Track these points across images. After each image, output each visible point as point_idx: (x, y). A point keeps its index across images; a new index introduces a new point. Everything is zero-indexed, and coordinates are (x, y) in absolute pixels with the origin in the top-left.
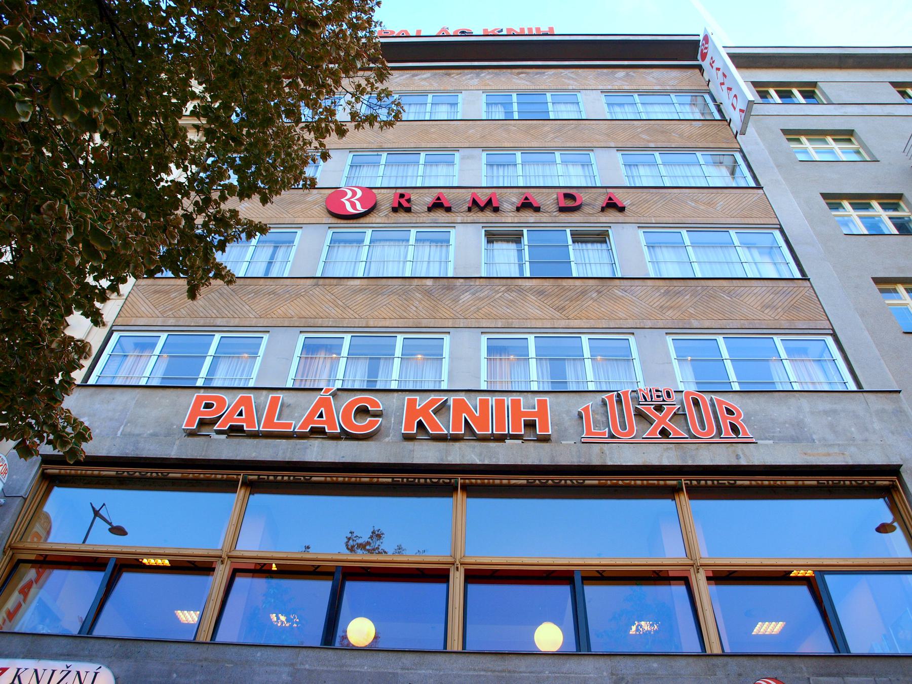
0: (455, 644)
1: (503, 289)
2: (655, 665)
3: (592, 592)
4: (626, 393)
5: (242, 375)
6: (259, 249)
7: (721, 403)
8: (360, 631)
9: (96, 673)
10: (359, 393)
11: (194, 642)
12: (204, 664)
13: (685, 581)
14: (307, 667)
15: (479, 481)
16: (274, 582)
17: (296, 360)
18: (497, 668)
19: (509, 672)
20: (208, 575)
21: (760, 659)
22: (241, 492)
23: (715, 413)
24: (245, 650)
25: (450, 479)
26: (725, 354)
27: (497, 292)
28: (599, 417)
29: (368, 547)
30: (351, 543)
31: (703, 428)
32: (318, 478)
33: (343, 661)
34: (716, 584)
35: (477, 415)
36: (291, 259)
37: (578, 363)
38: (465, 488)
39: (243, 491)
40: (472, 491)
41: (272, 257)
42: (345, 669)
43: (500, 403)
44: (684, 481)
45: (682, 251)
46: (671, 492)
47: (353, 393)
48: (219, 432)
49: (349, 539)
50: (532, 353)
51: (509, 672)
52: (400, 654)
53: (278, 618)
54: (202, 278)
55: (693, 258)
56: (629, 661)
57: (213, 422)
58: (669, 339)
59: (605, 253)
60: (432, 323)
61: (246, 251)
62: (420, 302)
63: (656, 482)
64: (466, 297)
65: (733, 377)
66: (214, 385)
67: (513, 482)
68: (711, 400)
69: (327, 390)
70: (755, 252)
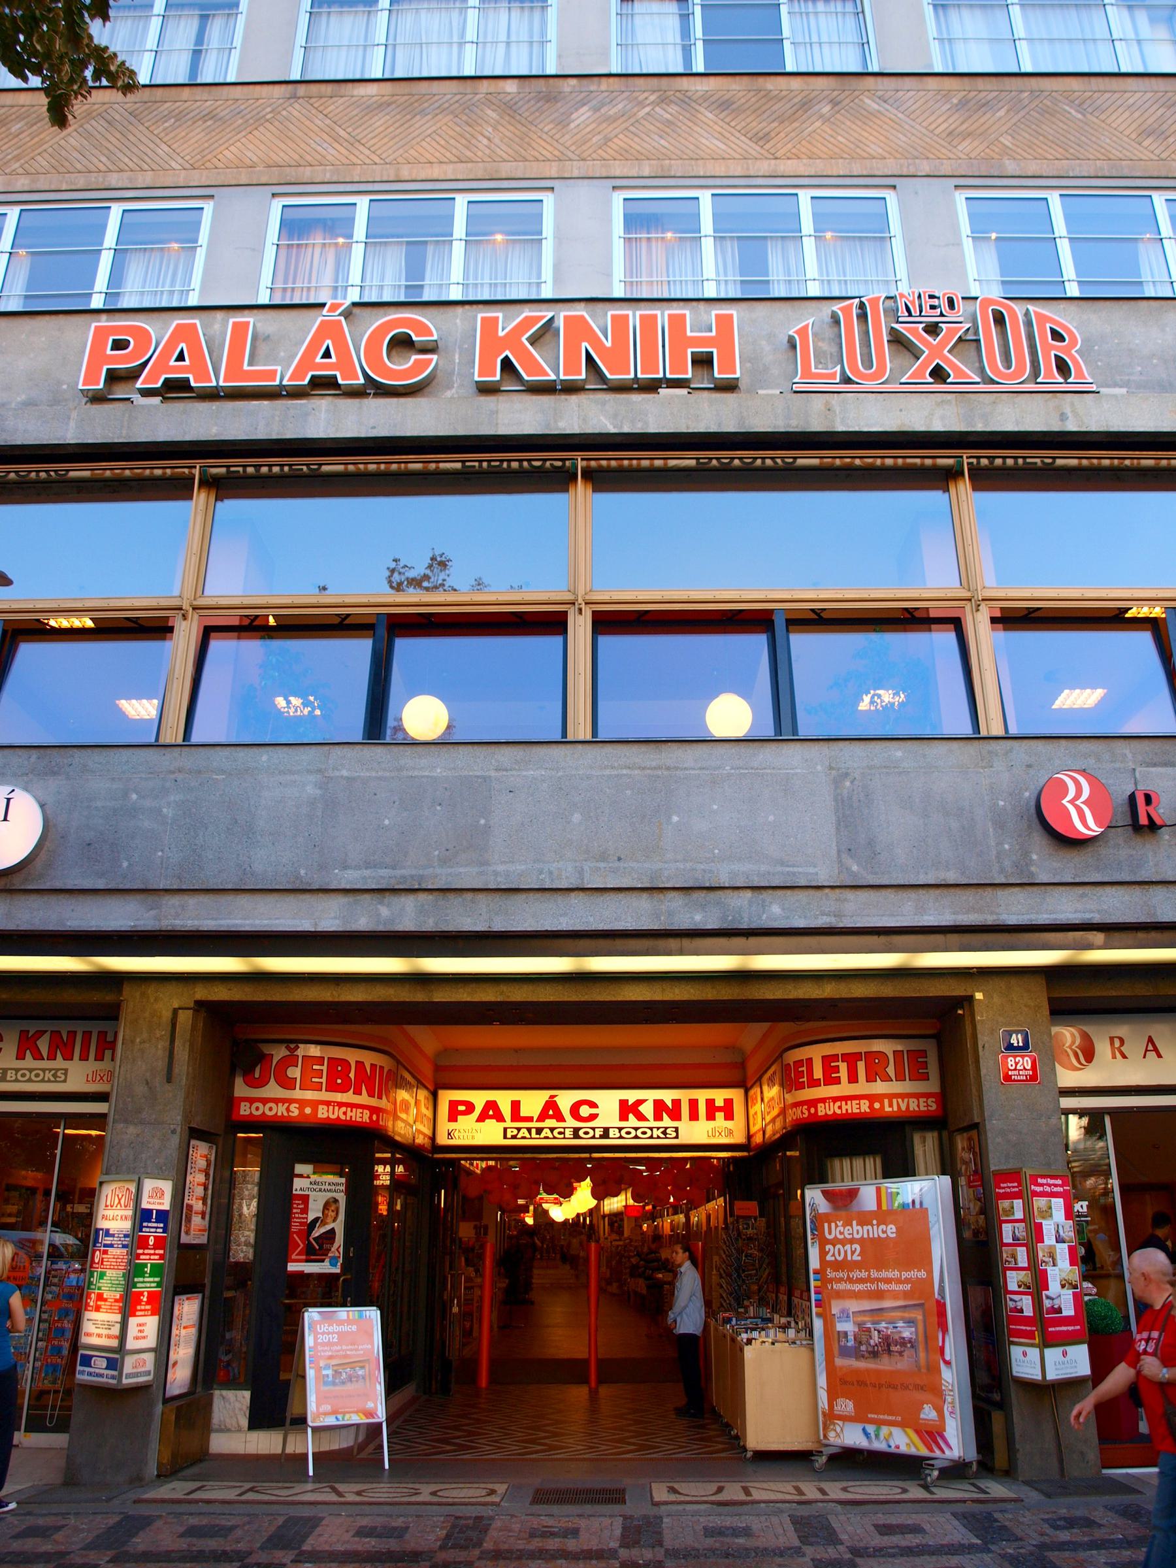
0: (580, 729)
1: (652, 98)
2: (899, 754)
3: (802, 644)
4: (874, 302)
5: (173, 283)
6: (171, 23)
7: (1042, 319)
8: (422, 715)
9: (9, 800)
10: (392, 309)
11: (157, 746)
12: (180, 777)
13: (956, 624)
14: (345, 773)
15: (613, 463)
16: (277, 644)
17: (270, 253)
18: (648, 764)
19: (668, 768)
20: (164, 639)
21: (1063, 742)
22: (201, 498)
23: (1031, 337)
24: (241, 753)
25: (563, 460)
26: (1060, 227)
27: (641, 104)
28: (824, 346)
29: (425, 584)
30: (396, 578)
31: (1007, 362)
32: (332, 466)
33: (402, 762)
34: (1005, 630)
35: (608, 344)
36: (238, 42)
37: (791, 245)
38: (588, 475)
39: (203, 495)
40: (601, 480)
41: (200, 38)
42: (405, 773)
43: (649, 323)
44: (967, 458)
45: (1000, 14)
46: (943, 478)
47: (381, 310)
48: (147, 393)
49: (393, 571)
50: (707, 224)
51: (668, 768)
52: (492, 749)
53: (289, 702)
54: (72, 81)
55: (1020, 32)
56: (858, 749)
57: (133, 375)
58: (960, 197)
59: (851, 22)
60: (519, 169)
61: (146, 29)
62: (495, 128)
63: (918, 461)
64: (583, 115)
65: (1069, 270)
66: (125, 306)
67: (672, 463)
68: (1027, 314)
69: (334, 307)
70: (1142, 17)
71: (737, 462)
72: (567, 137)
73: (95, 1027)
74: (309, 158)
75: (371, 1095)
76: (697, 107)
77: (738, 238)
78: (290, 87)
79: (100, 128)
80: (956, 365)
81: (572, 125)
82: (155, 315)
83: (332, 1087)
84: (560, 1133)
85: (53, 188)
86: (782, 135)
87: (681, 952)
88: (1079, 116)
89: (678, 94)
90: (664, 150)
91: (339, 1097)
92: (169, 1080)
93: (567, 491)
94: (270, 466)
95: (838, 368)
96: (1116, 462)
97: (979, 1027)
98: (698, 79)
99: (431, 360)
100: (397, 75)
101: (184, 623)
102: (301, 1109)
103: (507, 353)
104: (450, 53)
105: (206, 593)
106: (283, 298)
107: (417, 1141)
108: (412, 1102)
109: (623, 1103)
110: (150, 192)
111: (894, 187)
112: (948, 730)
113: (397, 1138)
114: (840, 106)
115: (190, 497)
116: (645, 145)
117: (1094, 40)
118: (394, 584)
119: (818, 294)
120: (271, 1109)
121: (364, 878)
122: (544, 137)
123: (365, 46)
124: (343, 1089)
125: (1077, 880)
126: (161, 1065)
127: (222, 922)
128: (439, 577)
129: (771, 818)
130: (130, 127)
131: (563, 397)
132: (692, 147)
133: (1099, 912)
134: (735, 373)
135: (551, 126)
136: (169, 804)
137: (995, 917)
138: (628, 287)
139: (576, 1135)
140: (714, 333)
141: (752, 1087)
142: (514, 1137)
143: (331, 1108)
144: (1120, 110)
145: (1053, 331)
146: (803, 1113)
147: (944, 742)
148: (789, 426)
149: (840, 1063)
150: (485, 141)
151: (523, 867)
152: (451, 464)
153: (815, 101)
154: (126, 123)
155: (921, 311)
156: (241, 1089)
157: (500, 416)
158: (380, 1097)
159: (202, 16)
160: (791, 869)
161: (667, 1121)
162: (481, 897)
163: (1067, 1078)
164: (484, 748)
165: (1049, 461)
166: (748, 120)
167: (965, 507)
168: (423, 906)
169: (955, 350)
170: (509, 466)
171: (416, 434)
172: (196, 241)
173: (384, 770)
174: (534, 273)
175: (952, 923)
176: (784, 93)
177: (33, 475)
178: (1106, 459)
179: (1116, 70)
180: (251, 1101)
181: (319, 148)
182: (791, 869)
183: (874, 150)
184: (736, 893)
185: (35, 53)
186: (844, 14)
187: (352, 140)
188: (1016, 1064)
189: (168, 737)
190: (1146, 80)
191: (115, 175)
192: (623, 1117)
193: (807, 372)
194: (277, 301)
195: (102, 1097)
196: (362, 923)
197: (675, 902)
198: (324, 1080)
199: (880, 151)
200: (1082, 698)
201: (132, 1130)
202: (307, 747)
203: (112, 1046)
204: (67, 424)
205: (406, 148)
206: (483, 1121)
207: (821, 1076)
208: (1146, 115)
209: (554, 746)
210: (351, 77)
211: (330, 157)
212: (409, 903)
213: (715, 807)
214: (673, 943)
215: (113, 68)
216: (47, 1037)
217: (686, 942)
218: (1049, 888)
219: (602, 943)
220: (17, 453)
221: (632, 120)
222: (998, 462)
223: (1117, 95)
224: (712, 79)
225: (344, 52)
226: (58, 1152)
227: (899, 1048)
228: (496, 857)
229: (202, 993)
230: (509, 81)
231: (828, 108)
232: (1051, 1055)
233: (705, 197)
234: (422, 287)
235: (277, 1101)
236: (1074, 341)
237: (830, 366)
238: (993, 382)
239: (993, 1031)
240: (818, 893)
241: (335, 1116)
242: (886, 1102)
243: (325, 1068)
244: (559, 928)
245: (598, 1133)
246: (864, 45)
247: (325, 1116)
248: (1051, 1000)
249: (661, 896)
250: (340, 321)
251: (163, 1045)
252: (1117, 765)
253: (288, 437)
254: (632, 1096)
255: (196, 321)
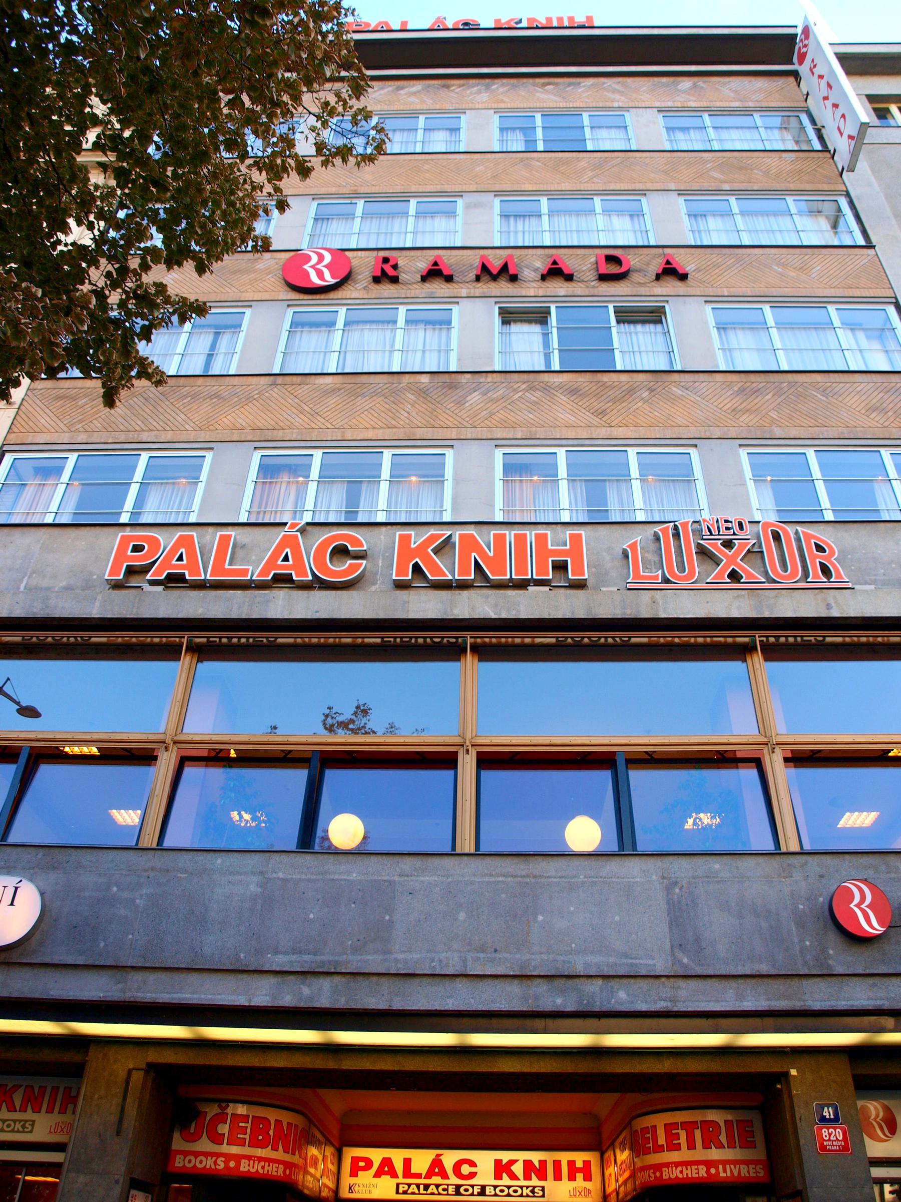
0: (466, 844)
1: (524, 386)
2: (717, 866)
3: (638, 778)
4: (685, 525)
5: (179, 507)
6: (194, 337)
7: (808, 537)
8: (344, 829)
9: (16, 888)
10: (335, 528)
11: (136, 848)
12: (152, 874)
13: (758, 763)
14: (281, 875)
15: (494, 640)
16: (235, 772)
18: (519, 873)
19: (535, 877)
20: (150, 765)
21: (847, 857)
22: (186, 660)
23: (800, 549)
24: (202, 857)
25: (457, 638)
26: (816, 473)
27: (516, 391)
28: (649, 556)
29: (351, 726)
31: (785, 569)
32: (285, 639)
33: (326, 868)
34: (795, 767)
35: (491, 554)
36: (239, 349)
37: (623, 486)
38: (475, 649)
39: (188, 658)
40: (485, 653)
42: (328, 877)
43: (520, 539)
44: (759, 637)
45: (763, 334)
46: (741, 652)
47: (327, 529)
48: (153, 583)
49: (327, 716)
50: (562, 471)
51: (535, 877)
52: (397, 858)
53: (241, 817)
54: (121, 378)
55: (778, 344)
56: (684, 862)
58: (743, 453)
59: (660, 338)
60: (429, 433)
61: (177, 341)
62: (413, 406)
63: (722, 639)
65: (825, 502)
66: (144, 522)
67: (538, 640)
68: (797, 533)
69: (293, 525)
70: (861, 335)
71: (586, 640)
72: (463, 412)
73: (62, 1083)
74: (281, 424)
75: (286, 1151)
76: (555, 393)
77: (585, 480)
78: (272, 378)
79: (139, 403)
80: (748, 570)
81: (467, 404)
82: (165, 528)
83: (254, 1144)
84: (444, 1190)
85: (102, 441)
86: (615, 411)
87: (545, 1031)
88: (824, 398)
89: (541, 384)
90: (532, 421)
91: (259, 1152)
92: (118, 1133)
93: (459, 660)
94: (239, 638)
95: (660, 572)
96: (871, 639)
97: (795, 1100)
98: (555, 374)
99: (361, 564)
100: (346, 371)
101: (166, 754)
102: (226, 1163)
103: (417, 560)
104: (383, 358)
105: (184, 731)
106: (257, 519)
107: (323, 1194)
108: (320, 1158)
109: (498, 1162)
110: (170, 444)
111: (696, 446)
112: (756, 846)
113: (306, 1191)
114: (655, 392)
115: (177, 658)
116: (519, 418)
117: (830, 350)
118: (328, 726)
119: (643, 520)
120: (201, 1162)
121: (291, 962)
122: (448, 411)
123: (325, 353)
124: (263, 1146)
125: (868, 972)
126: (113, 1119)
127: (175, 996)
128: (361, 721)
129: (617, 918)
130: (160, 403)
131: (457, 592)
132: (552, 419)
133: (887, 999)
134: (584, 575)
135: (452, 404)
136: (141, 896)
137: (802, 1003)
138: (506, 515)
139: (458, 1193)
140: (568, 547)
141: (606, 1151)
142: (405, 1192)
143: (252, 1162)
144: (853, 394)
145: (817, 545)
146: (649, 1177)
147: (753, 857)
148: (625, 614)
149: (680, 1131)
150: (406, 414)
151: (418, 956)
152: (373, 639)
153: (637, 389)
154: (157, 400)
155: (719, 531)
156: (178, 1143)
157: (410, 605)
158: (293, 1154)
159: (216, 333)
160: (634, 961)
161: (535, 1181)
162: (384, 980)
163: (876, 1149)
164: (391, 857)
165: (821, 639)
166: (591, 401)
167: (759, 673)
168: (337, 986)
169: (746, 559)
170: (416, 641)
171: (348, 617)
172: (198, 478)
173: (312, 873)
174: (438, 504)
175: (767, 1008)
176: (615, 384)
177: (65, 639)
178: (863, 637)
179: (847, 369)
180: (186, 1153)
181: (289, 418)
182: (634, 961)
183: (680, 421)
184: (590, 981)
185: (99, 361)
186: (656, 333)
187: (313, 413)
188: (830, 1135)
189: (146, 842)
190: (868, 375)
191: (146, 434)
192: (498, 1176)
193: (637, 575)
194: (253, 521)
195: (59, 1147)
196: (288, 1000)
197: (541, 988)
198: (247, 1136)
199: (685, 422)
200: (861, 819)
201: (82, 1179)
202: (253, 854)
203: (74, 1100)
204: (94, 604)
205: (350, 418)
206: (380, 1177)
207: (664, 1143)
208: (871, 397)
209: (446, 857)
210: (314, 372)
211: (296, 424)
212: (326, 984)
213: (572, 909)
214: (539, 1023)
215: (150, 371)
216: (21, 1091)
217: (549, 1022)
218: (845, 979)
219: (482, 1022)
220: (56, 623)
221: (510, 401)
222: (782, 639)
223: (848, 385)
224: (565, 375)
225: (311, 355)
226: (17, 1196)
227: (729, 1117)
228: (397, 947)
229: (153, 1056)
230: (424, 375)
231: (647, 393)
232: (858, 1128)
233: (561, 453)
234: (357, 512)
235: (207, 1154)
236: (832, 552)
237: (654, 570)
238: (775, 582)
239: (807, 1104)
240: (656, 982)
241: (254, 1170)
242: (721, 1167)
243: (249, 1125)
244: (446, 1008)
245: (477, 1190)
246: (670, 353)
247: (246, 1169)
248: (854, 1077)
249: (529, 982)
250: (297, 536)
251: (117, 1101)
252: (893, 875)
253: (254, 617)
254: (505, 1156)
255: (194, 533)
